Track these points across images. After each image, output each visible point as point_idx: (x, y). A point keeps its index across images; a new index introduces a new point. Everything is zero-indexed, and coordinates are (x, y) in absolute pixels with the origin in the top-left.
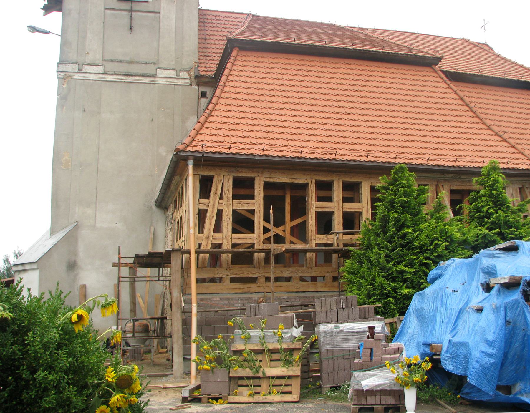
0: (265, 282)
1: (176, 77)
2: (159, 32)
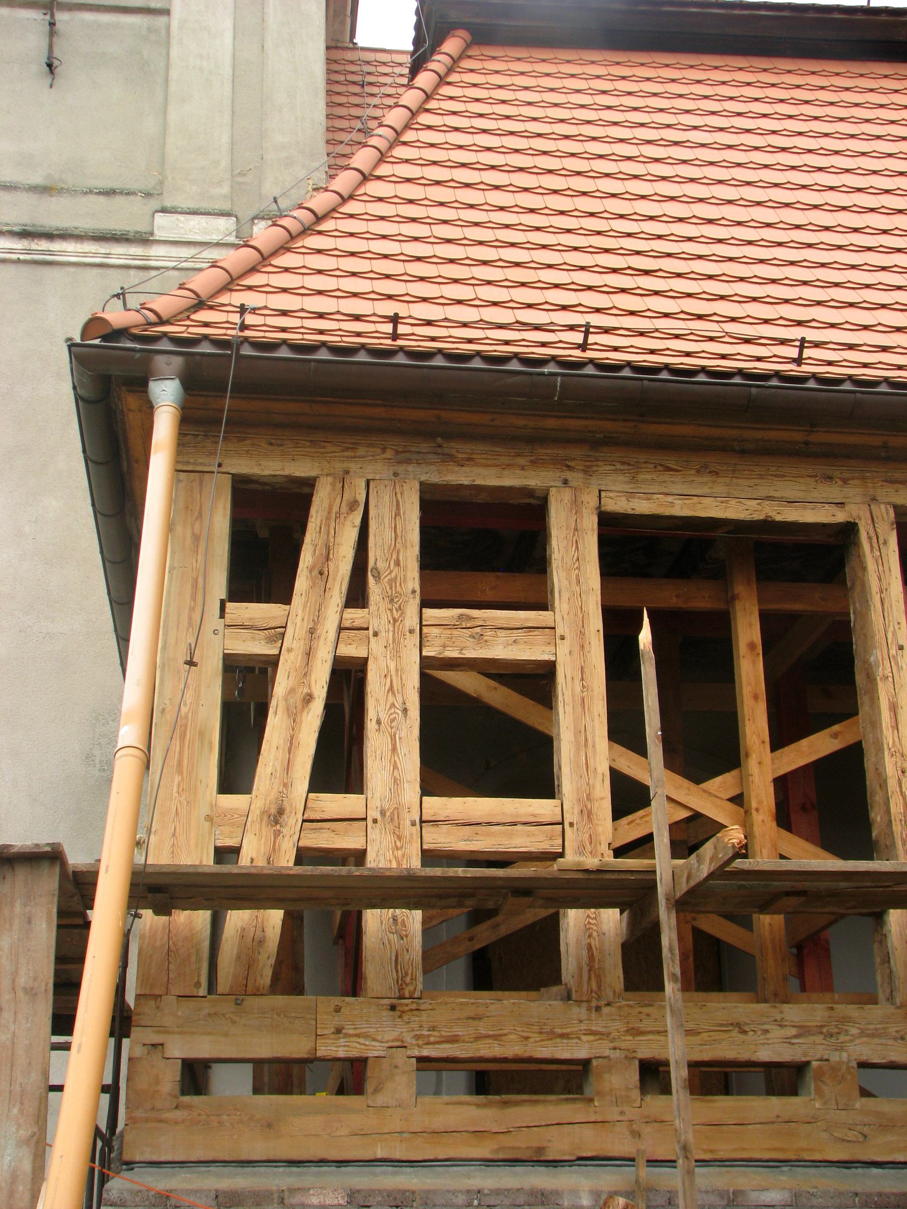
0: (636, 1094)
1: (232, 239)
2: (167, 80)
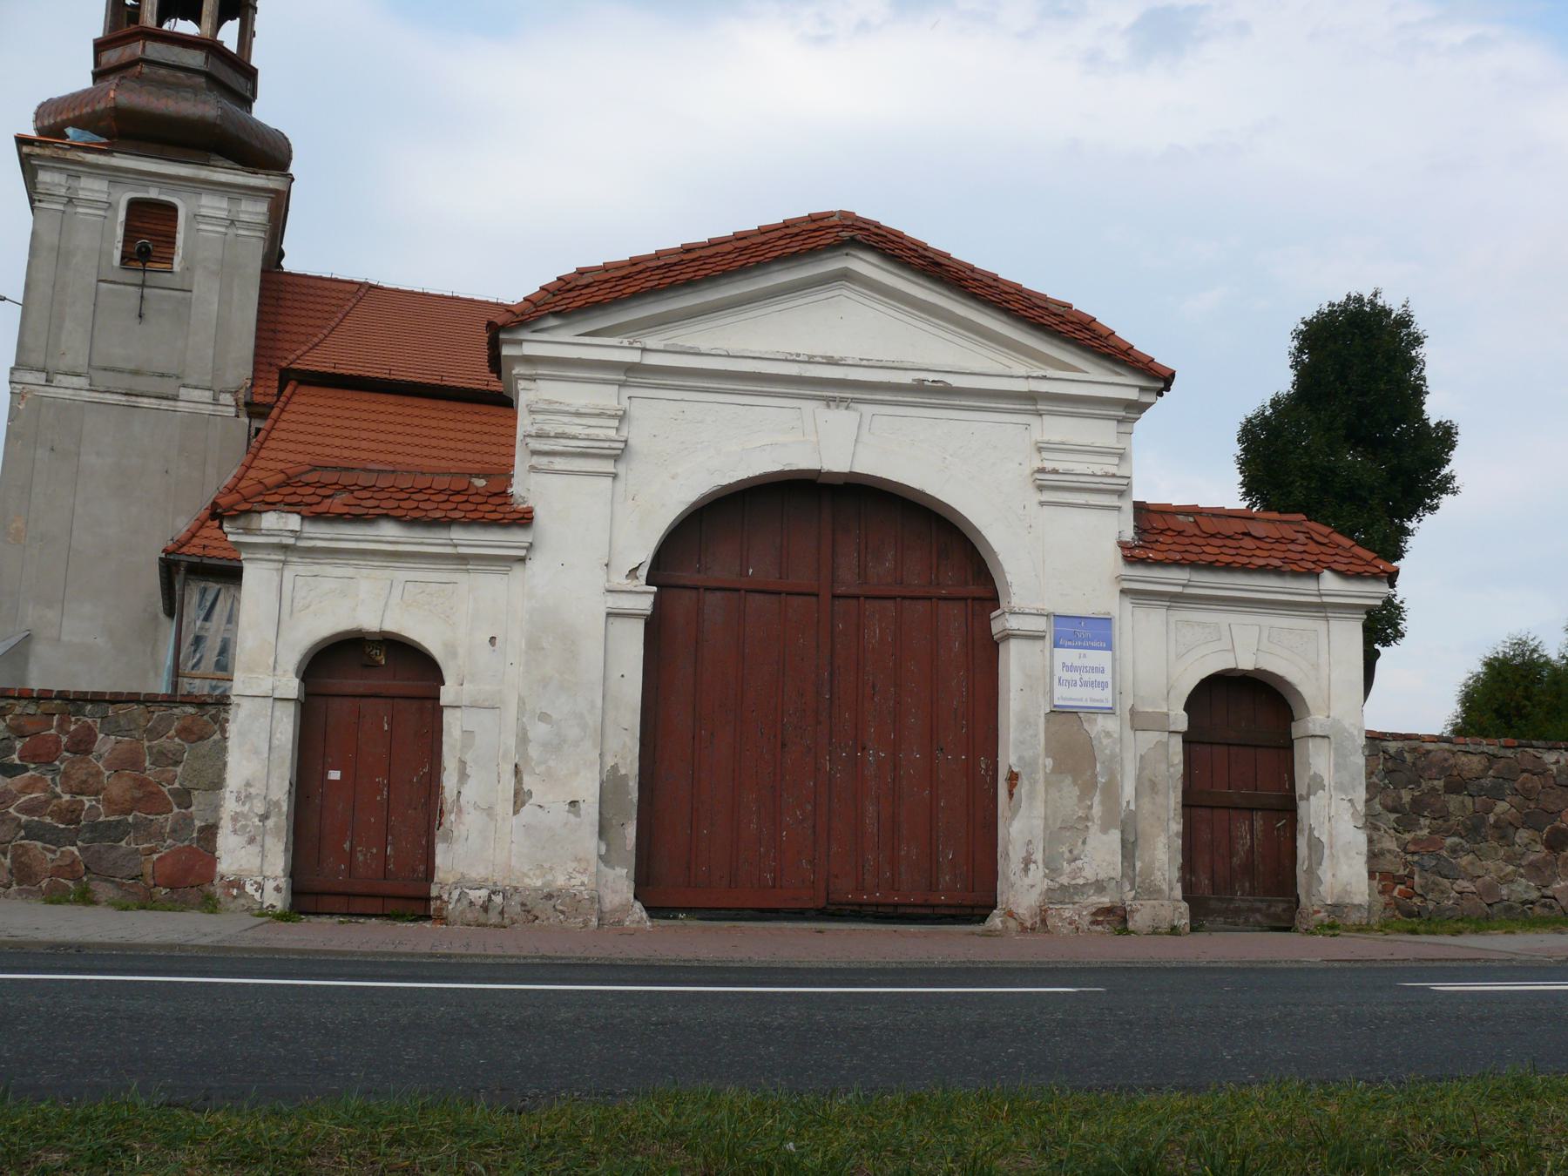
1: (211, 401)
